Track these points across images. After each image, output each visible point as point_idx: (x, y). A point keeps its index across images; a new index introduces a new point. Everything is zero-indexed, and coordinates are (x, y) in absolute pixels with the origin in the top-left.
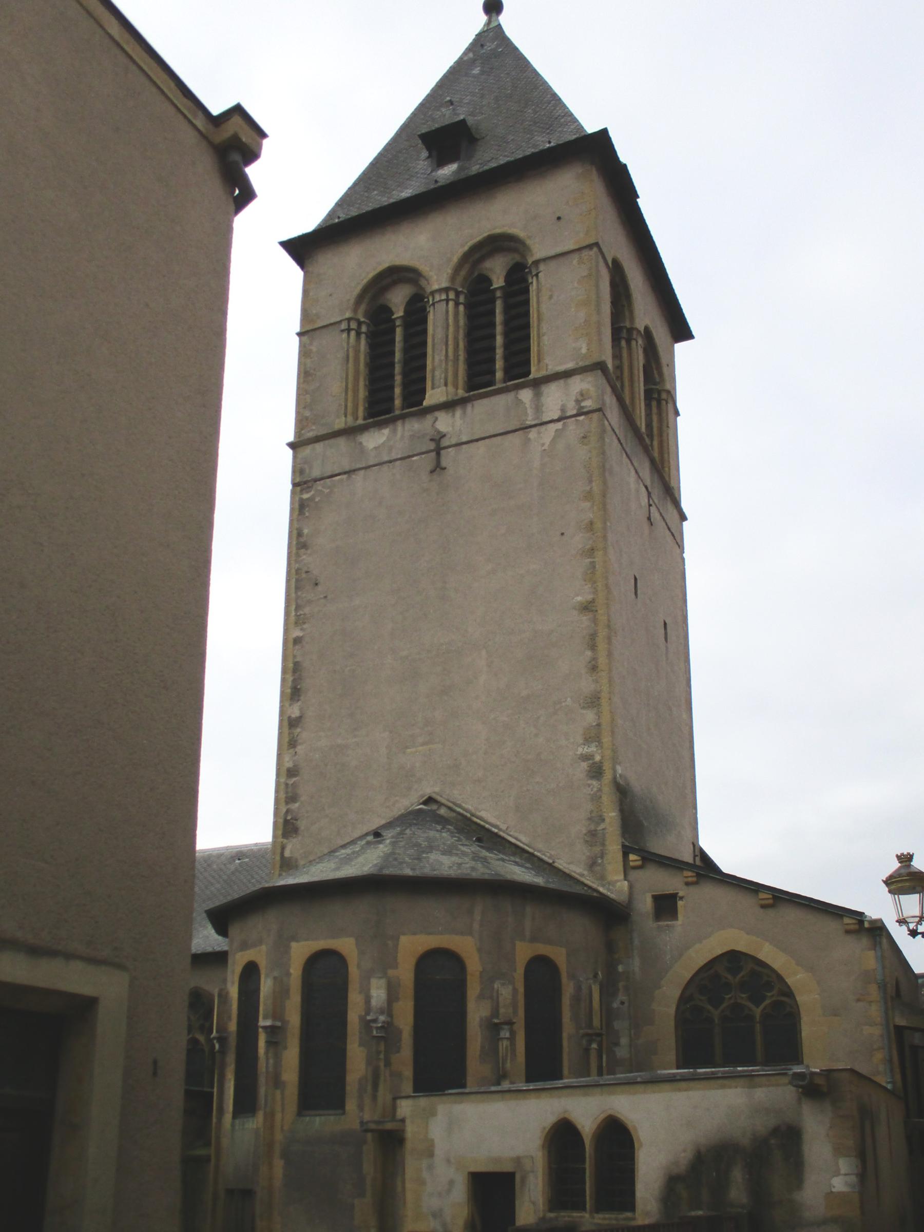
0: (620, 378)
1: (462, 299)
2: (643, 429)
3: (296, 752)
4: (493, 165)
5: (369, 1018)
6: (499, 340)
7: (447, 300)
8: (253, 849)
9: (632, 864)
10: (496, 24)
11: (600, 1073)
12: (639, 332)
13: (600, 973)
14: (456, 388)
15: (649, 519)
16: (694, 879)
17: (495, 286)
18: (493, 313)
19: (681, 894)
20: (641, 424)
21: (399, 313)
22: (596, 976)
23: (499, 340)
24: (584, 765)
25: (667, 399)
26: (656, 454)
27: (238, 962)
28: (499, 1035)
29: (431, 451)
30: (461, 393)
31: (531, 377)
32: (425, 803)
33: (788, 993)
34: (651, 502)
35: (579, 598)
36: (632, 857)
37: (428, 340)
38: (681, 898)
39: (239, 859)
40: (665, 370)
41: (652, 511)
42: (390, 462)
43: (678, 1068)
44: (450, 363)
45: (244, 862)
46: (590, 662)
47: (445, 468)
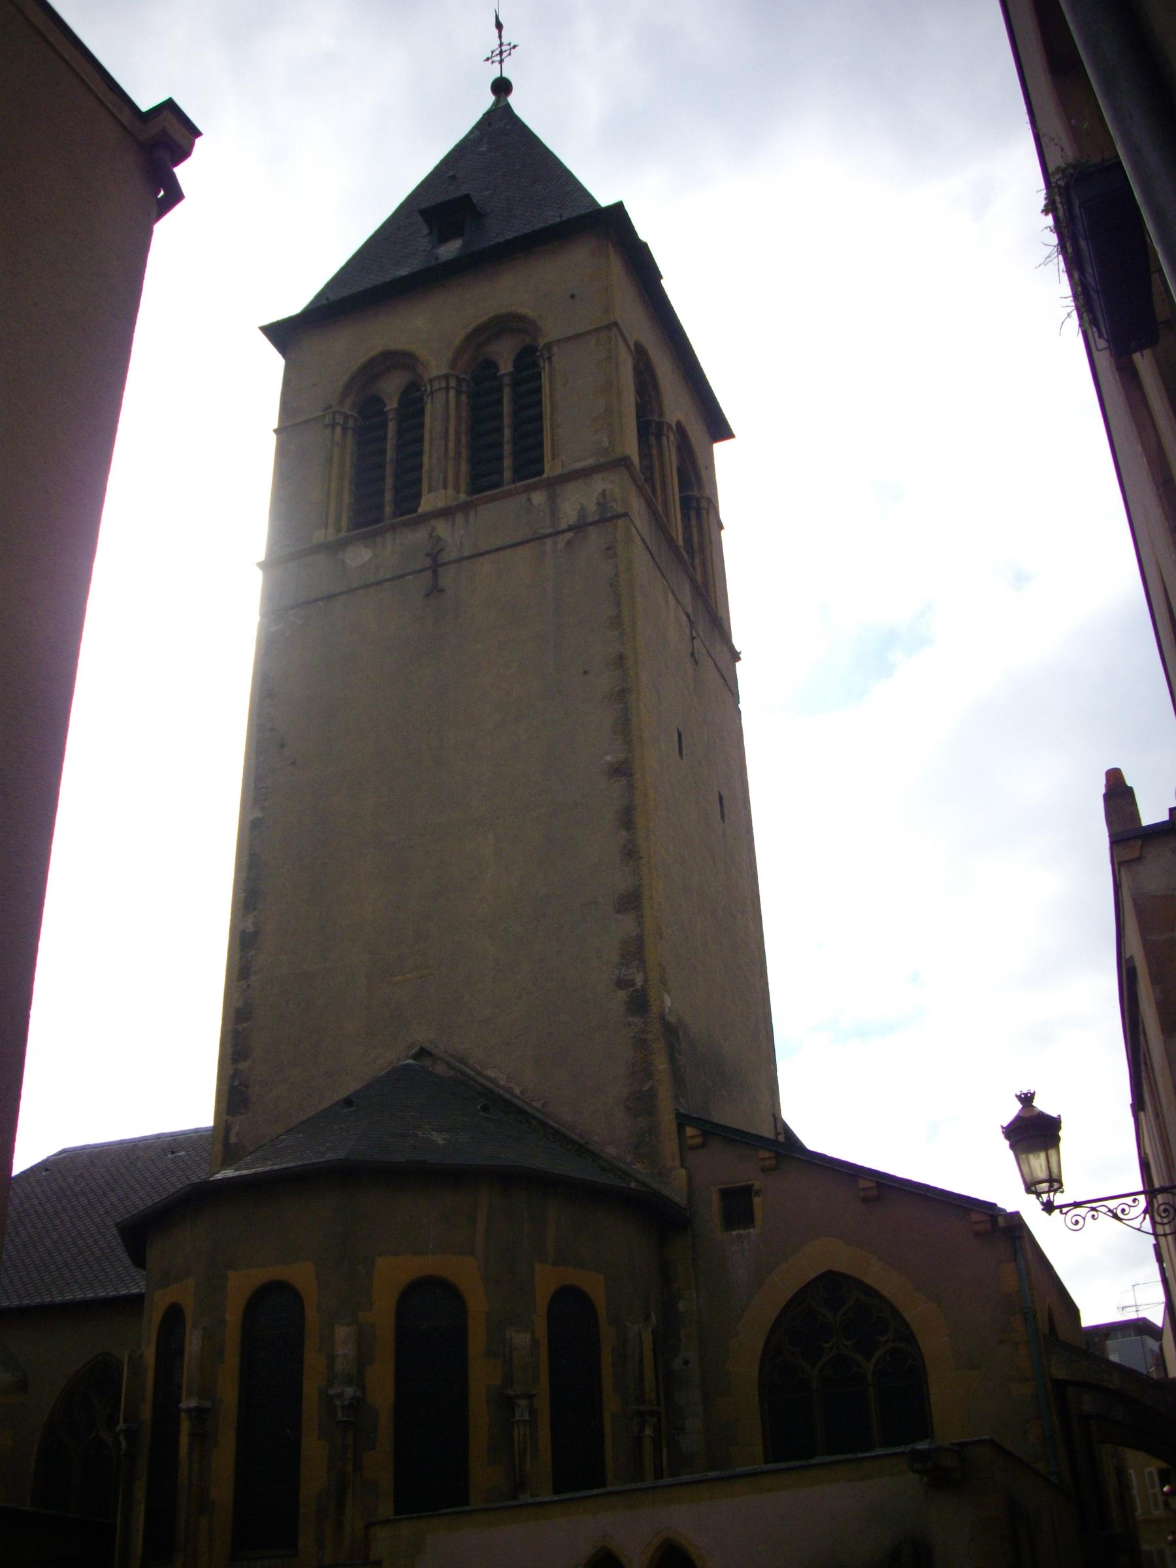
0: (650, 480)
1: (464, 388)
2: (681, 542)
3: (248, 986)
4: (500, 239)
5: (330, 1392)
6: (507, 433)
7: (447, 389)
8: (191, 1137)
9: (690, 1142)
10: (505, 103)
11: (658, 1474)
12: (670, 427)
13: (653, 1314)
14: (458, 491)
15: (692, 654)
16: (772, 1162)
17: (502, 372)
18: (499, 402)
19: (757, 1185)
20: (677, 536)
21: (392, 405)
22: (647, 1317)
23: (507, 433)
24: (622, 995)
25: (708, 508)
26: (699, 578)
27: (159, 1303)
28: (514, 1416)
29: (427, 569)
30: (463, 497)
31: (545, 476)
32: (416, 1057)
33: (907, 1335)
34: (694, 634)
35: (609, 758)
36: (690, 1131)
37: (425, 435)
38: (757, 1193)
39: (173, 1153)
40: (704, 474)
41: (695, 646)
42: (378, 583)
43: (766, 1463)
44: (451, 463)
45: (179, 1156)
46: (625, 846)
47: (442, 590)
